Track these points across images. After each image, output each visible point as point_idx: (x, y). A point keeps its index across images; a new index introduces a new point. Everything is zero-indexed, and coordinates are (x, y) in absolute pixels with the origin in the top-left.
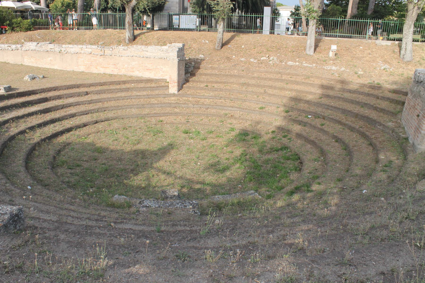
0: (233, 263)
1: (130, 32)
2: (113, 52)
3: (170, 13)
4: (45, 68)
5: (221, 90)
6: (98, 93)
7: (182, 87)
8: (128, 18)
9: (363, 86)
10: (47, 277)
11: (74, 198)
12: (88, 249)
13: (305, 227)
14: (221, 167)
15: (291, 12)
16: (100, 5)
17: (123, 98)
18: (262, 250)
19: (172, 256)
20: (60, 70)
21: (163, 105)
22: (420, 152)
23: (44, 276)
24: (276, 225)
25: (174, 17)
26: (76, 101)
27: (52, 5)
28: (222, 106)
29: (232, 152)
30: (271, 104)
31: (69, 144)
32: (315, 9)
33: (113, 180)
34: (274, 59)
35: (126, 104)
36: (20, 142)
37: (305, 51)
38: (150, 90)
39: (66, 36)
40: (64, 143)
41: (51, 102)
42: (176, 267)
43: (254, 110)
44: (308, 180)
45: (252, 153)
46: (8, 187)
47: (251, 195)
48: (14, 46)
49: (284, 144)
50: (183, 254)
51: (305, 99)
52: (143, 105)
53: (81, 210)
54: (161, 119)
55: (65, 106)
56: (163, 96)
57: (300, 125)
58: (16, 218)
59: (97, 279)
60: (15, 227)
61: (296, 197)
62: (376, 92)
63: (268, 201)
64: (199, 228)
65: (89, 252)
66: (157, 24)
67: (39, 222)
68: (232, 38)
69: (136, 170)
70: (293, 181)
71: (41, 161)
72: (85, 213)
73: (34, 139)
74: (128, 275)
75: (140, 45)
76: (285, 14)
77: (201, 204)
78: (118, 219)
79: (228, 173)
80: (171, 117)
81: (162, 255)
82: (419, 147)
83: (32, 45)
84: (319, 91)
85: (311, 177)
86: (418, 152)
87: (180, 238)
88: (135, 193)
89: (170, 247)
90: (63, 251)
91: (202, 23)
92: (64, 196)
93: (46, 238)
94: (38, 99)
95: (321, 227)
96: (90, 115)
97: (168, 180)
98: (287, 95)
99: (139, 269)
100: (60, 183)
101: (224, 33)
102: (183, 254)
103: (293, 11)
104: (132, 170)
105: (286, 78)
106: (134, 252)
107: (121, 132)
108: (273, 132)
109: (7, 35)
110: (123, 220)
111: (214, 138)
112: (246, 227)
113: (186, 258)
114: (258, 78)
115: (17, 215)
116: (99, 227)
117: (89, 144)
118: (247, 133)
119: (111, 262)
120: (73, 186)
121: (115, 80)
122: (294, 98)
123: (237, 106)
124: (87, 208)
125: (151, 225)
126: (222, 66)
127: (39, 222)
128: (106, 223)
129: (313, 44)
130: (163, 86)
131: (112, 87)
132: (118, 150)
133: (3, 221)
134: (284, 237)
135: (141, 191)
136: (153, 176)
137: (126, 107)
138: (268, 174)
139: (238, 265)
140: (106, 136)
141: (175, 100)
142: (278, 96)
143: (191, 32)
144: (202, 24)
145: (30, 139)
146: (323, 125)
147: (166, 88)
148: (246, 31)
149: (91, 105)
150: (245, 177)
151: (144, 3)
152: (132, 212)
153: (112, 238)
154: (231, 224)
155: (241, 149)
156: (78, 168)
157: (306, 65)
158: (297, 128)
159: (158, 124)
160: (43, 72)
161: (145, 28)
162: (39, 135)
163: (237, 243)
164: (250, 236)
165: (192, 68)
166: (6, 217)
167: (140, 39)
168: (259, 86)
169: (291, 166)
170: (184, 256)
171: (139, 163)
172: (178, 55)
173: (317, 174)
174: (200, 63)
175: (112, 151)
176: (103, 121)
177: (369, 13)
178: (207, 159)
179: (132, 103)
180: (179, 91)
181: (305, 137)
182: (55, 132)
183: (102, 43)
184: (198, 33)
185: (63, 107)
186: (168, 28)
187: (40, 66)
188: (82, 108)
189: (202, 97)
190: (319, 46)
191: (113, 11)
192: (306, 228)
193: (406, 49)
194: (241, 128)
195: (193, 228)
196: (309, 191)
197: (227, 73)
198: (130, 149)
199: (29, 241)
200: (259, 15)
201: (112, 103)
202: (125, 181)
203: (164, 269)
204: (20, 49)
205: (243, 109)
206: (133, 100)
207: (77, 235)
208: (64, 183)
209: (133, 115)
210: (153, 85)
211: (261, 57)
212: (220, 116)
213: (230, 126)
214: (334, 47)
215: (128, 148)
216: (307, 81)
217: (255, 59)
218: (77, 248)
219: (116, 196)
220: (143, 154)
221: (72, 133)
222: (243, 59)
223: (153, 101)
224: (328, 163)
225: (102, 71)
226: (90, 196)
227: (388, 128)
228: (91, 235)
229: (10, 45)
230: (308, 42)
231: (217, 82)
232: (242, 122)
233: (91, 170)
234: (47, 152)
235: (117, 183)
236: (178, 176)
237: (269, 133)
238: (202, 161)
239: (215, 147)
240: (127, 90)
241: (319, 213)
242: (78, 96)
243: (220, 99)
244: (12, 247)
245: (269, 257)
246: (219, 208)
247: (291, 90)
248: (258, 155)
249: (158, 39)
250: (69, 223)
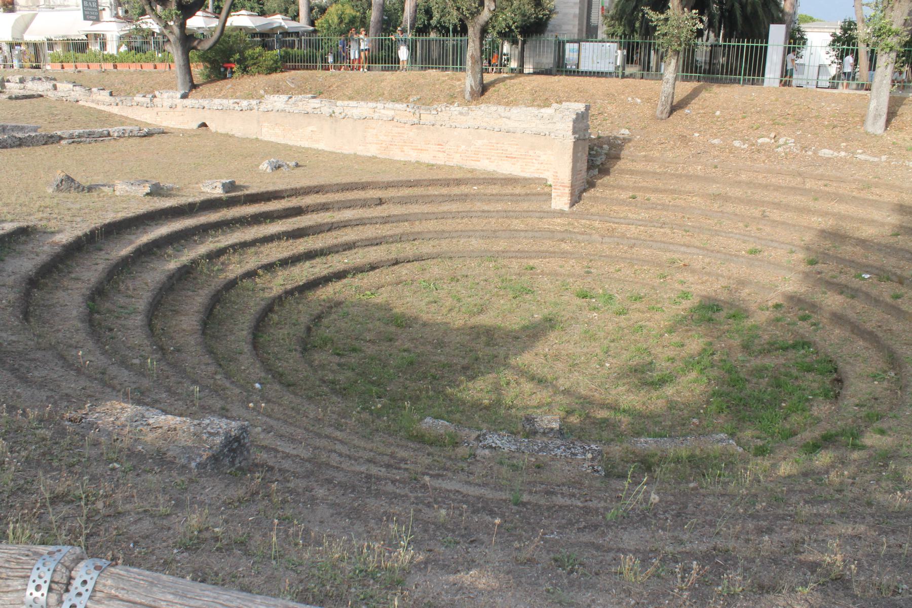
0: (681, 589)
1: (474, 78)
2: (438, 118)
3: (561, 38)
4: (300, 147)
5: (664, 207)
6: (403, 201)
7: (580, 198)
8: (472, 48)
10: (292, 569)
11: (344, 414)
12: (372, 524)
13: (847, 529)
14: (656, 375)
15: (834, 35)
16: (414, 20)
17: (454, 215)
18: (746, 569)
19: (545, 558)
20: (330, 152)
21: (537, 234)
23: (287, 568)
24: (777, 517)
25: (568, 46)
26: (359, 216)
27: (319, 21)
28: (664, 242)
29: (683, 346)
30: (776, 245)
31: (339, 304)
32: (894, 28)
33: (422, 384)
34: (788, 142)
35: (460, 227)
36: (246, 293)
37: (862, 126)
38: (512, 201)
39: (344, 84)
40: (329, 300)
41: (309, 216)
42: (556, 584)
43: (736, 256)
44: (854, 422)
45: (726, 350)
46: (219, 382)
47: (719, 443)
48: (244, 103)
49: (802, 337)
50: (569, 557)
51: (857, 234)
52: (495, 231)
53: (356, 442)
54: (532, 263)
55: (335, 225)
56: (537, 214)
57: (841, 293)
58: (236, 444)
59: (389, 589)
60: (232, 463)
61: (823, 458)
63: (759, 460)
64: (602, 504)
65: (373, 530)
66: (532, 60)
67: (276, 457)
68: (694, 94)
69: (473, 369)
70: (818, 420)
71: (282, 333)
72: (365, 449)
73: (271, 288)
74: (453, 587)
75: (494, 104)
76: (819, 44)
77: (607, 453)
78: (430, 469)
79: (669, 390)
80: (552, 260)
81: (525, 555)
83: (278, 101)
84: (894, 219)
85: (863, 414)
87: (564, 521)
88: (467, 416)
89: (542, 539)
90: (321, 522)
91: (629, 60)
92: (325, 409)
93: (291, 492)
94: (284, 210)
95: (887, 533)
96: (383, 247)
97: (539, 396)
98: (815, 225)
99: (477, 579)
100: (317, 382)
101: (677, 82)
102: (569, 557)
103: (839, 32)
104: (465, 368)
105: (815, 187)
106: (465, 542)
107: (445, 286)
108: (777, 306)
109: (234, 81)
110: (441, 472)
111: (643, 312)
112: (707, 514)
113: (576, 567)
114: (749, 184)
115: (237, 439)
116: (394, 482)
117: (379, 307)
118: (717, 306)
119: (421, 557)
120: (343, 392)
121: (440, 177)
122: (830, 233)
124: (369, 439)
125: (499, 488)
126: (670, 155)
127: (276, 457)
128: (406, 475)
129: (885, 110)
130: (539, 194)
131: (432, 191)
132: (437, 324)
133: (211, 448)
134: (796, 546)
135: (481, 413)
136: (508, 384)
137: (459, 233)
138: (759, 400)
139: (691, 596)
140: (415, 292)
142: (794, 226)
143: (603, 80)
144: (628, 63)
145: (263, 290)
146: (897, 297)
147: (545, 198)
148: (726, 79)
149: (388, 226)
150: (708, 402)
151: (507, 17)
152: (459, 456)
153: (420, 506)
154: (673, 503)
155: (702, 340)
156: (353, 355)
157: (863, 157)
158: (833, 301)
159: (524, 274)
160: (296, 155)
161: (506, 69)
162: (282, 282)
163: (688, 547)
164: (718, 533)
165: (604, 157)
166: (218, 440)
167: (495, 91)
168: (749, 202)
169: (815, 385)
170: (571, 561)
171: (480, 354)
172: (574, 128)
173: (878, 409)
174: (620, 147)
175: (425, 325)
176: (409, 262)
178: (625, 355)
179: (471, 227)
180: (572, 205)
182: (312, 277)
183: (415, 98)
184: (620, 82)
185: (331, 227)
186: (555, 70)
187: (290, 143)
188: (369, 232)
189: (622, 221)
190: (899, 113)
191: (440, 32)
192: (850, 531)
194: (704, 293)
195: (590, 504)
196: (855, 447)
197: (680, 171)
198: (462, 322)
199: (257, 493)
201: (431, 225)
202: (449, 390)
203: (530, 584)
204: (256, 107)
205: (712, 251)
206: (475, 220)
207: (351, 493)
208: (324, 382)
209: (473, 251)
210: (518, 190)
211: (759, 138)
212: (660, 265)
213: (680, 287)
215: (458, 320)
217: (744, 141)
218: (350, 518)
219: (428, 420)
220: (489, 335)
221: (345, 281)
222: (716, 141)
223: (517, 224)
224: (906, 386)
225: (412, 156)
226: (378, 415)
228: (378, 495)
229: (237, 101)
230: (873, 105)
231: (655, 190)
232: (707, 281)
233: (380, 360)
234: (295, 317)
235: (431, 393)
236: (562, 388)
237: (768, 309)
238: (615, 361)
239: (645, 331)
240: (464, 198)
241: (881, 499)
242: (363, 206)
243: (661, 227)
244: (228, 501)
245: (761, 587)
246: (646, 464)
247: (825, 214)
248: (740, 356)
249: (534, 92)
250: (333, 467)
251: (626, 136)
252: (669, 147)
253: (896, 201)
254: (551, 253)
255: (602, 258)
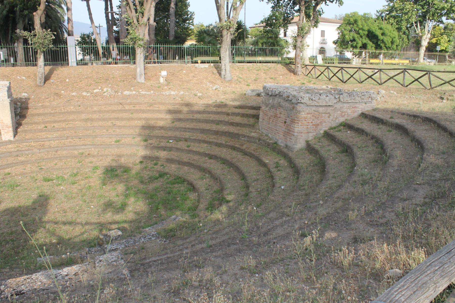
5: (64, 129)
9: (208, 106)
22: (296, 150)
30: (125, 136)
34: (108, 91)
43: (110, 145)
51: (158, 125)
54: (7, 171)
57: (164, 150)
62: (224, 110)
82: (295, 146)
84: (169, 116)
86: (295, 150)
98: (139, 125)
108: (141, 162)
114: (100, 112)
122: (147, 127)
123: (89, 143)
126: (55, 103)
141: (15, 148)
142: (130, 126)
146: (188, 146)
157: (143, 93)
177: (171, 38)
180: (15, 136)
181: (177, 161)
189: (46, 140)
193: (225, 70)
200: (62, 45)
205: (98, 145)
211: (94, 90)
212: (75, 157)
214: (164, 73)
216: (151, 108)
217: (88, 92)
222: (74, 94)
227: (254, 138)
230: (138, 70)
231: (55, 122)
247: (140, 119)
251: (26, 97)
252: (52, 100)
253: (166, 108)
254: (15, 163)
255: (45, 160)
